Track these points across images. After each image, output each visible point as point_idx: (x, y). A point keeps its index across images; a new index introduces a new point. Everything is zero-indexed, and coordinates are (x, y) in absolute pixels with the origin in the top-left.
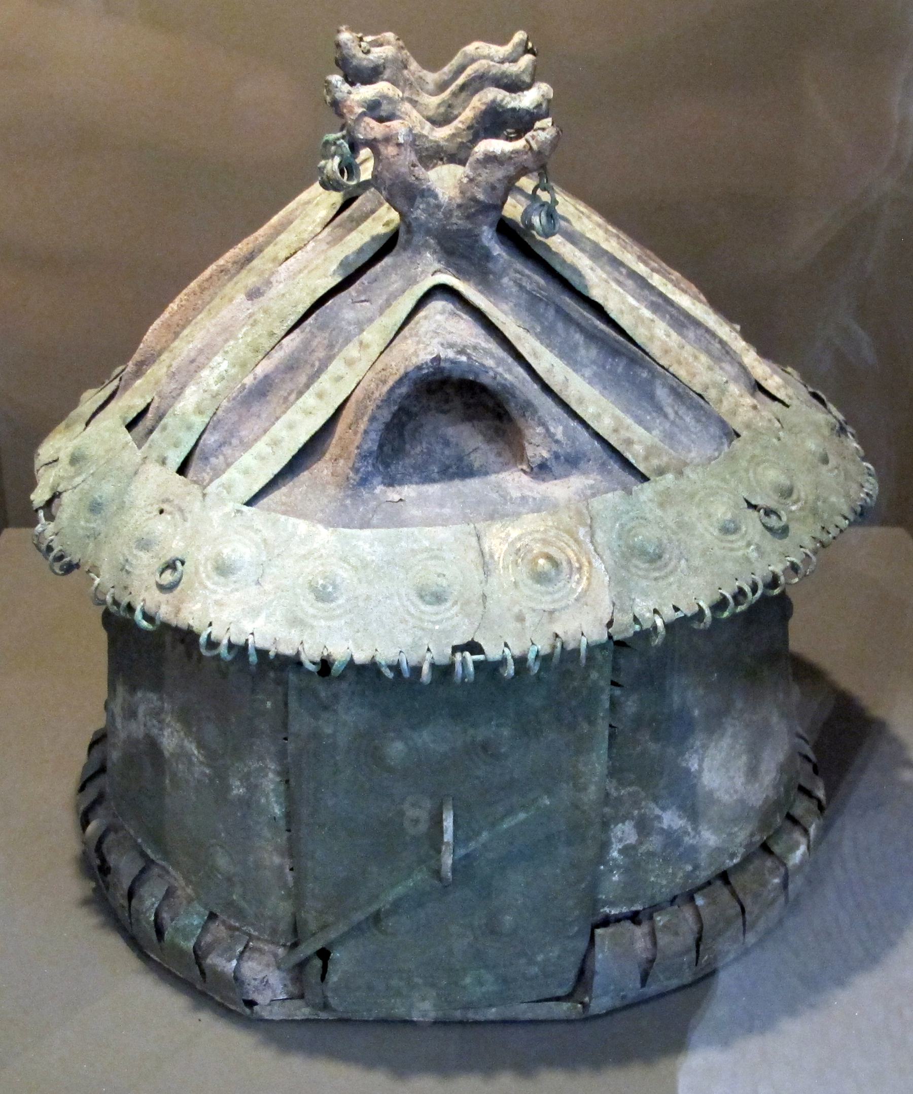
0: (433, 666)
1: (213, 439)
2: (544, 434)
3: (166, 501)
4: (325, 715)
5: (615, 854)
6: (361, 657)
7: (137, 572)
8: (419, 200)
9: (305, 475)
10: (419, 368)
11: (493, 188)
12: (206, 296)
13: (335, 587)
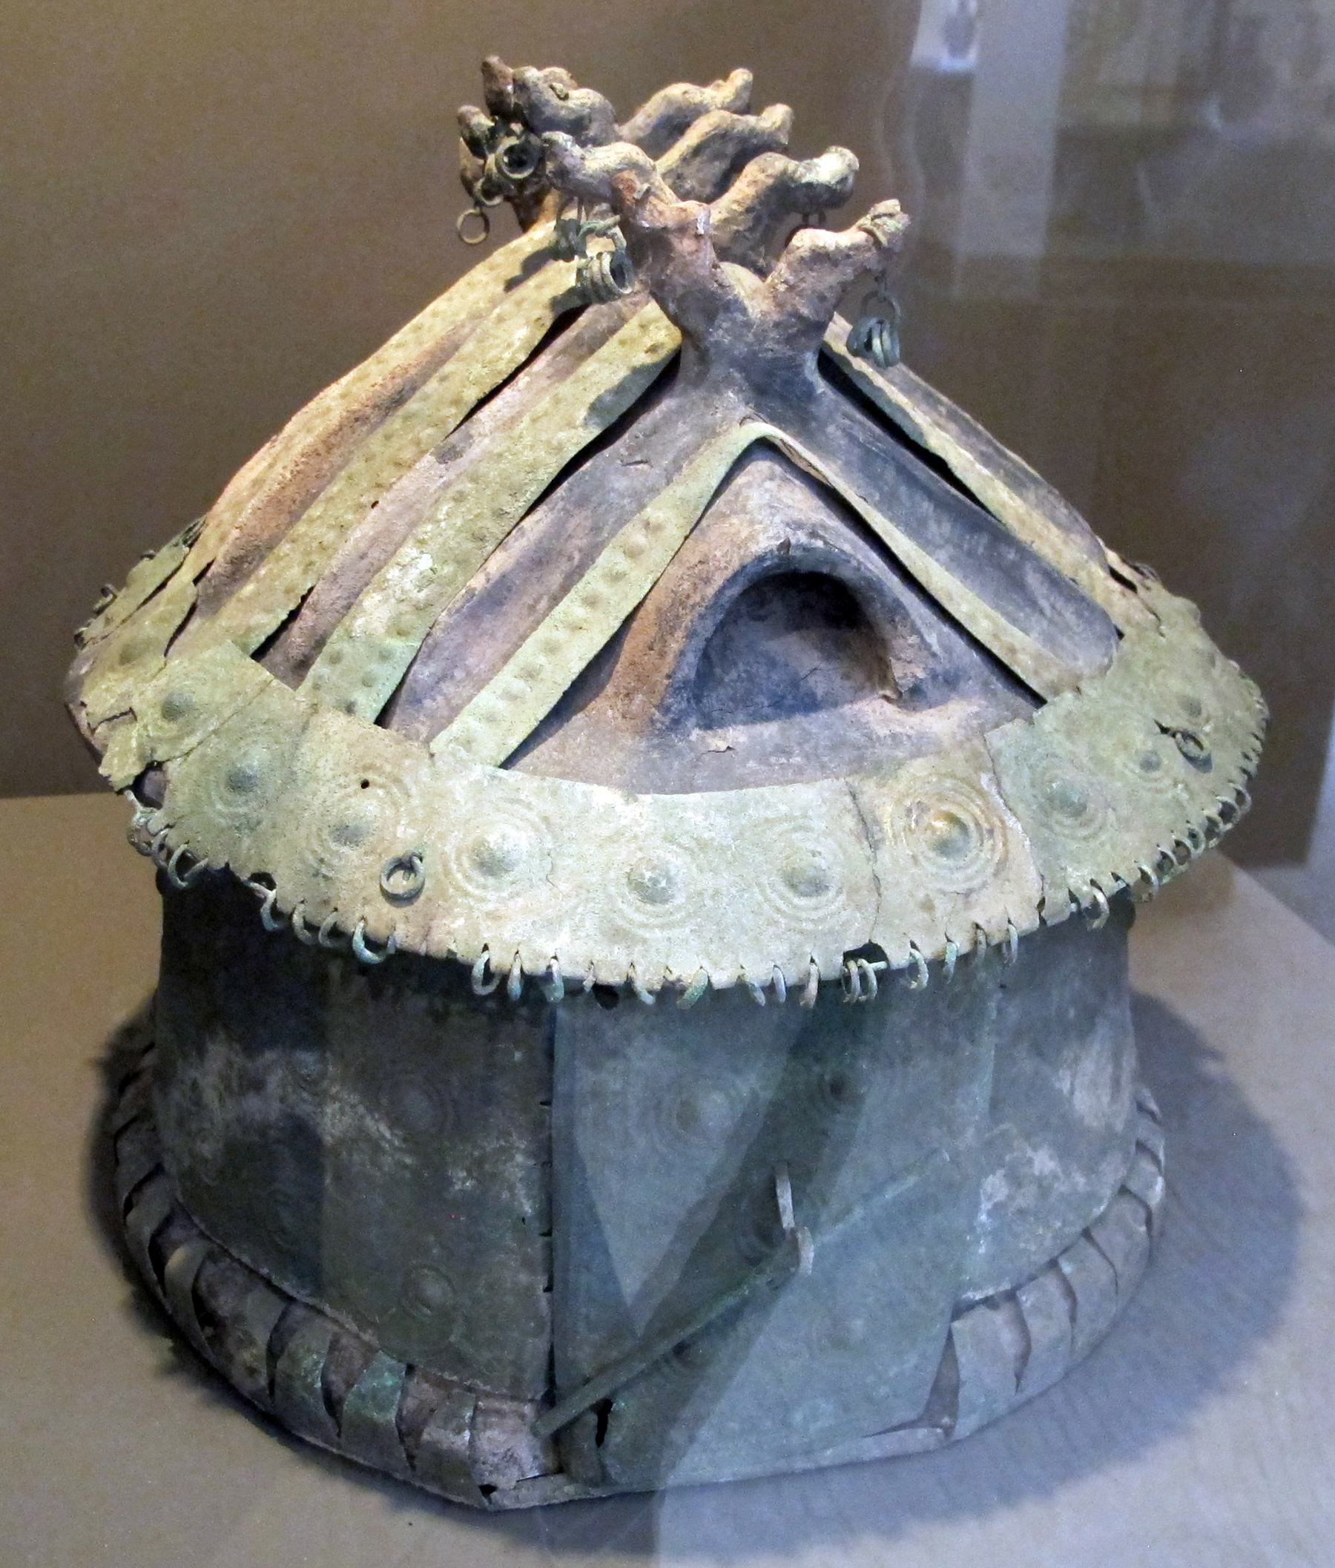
0: (822, 984)
1: (427, 673)
2: (918, 646)
4: (610, 1064)
5: (983, 1217)
6: (722, 979)
7: (344, 877)
8: (721, 316)
9: (578, 719)
10: (761, 559)
11: (822, 298)
12: (335, 458)
13: (669, 880)
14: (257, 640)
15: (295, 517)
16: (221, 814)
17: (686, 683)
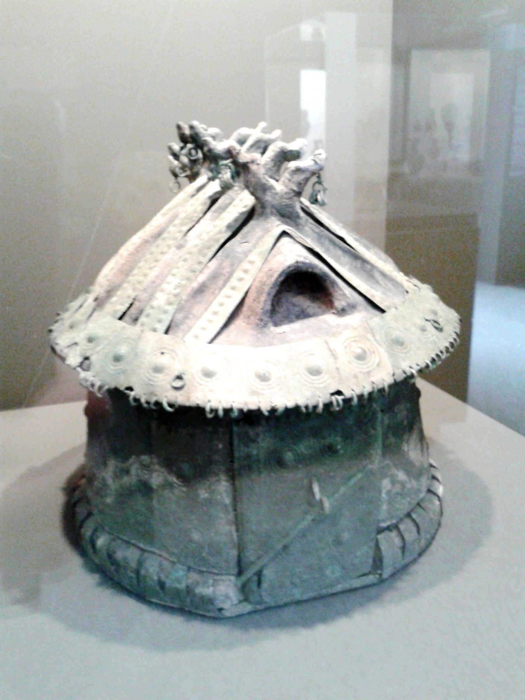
2: (343, 295)
3: (163, 348)
4: (252, 445)
6: (290, 404)
14: (120, 314)
15: (127, 275)
16: (112, 370)
17: (267, 311)
